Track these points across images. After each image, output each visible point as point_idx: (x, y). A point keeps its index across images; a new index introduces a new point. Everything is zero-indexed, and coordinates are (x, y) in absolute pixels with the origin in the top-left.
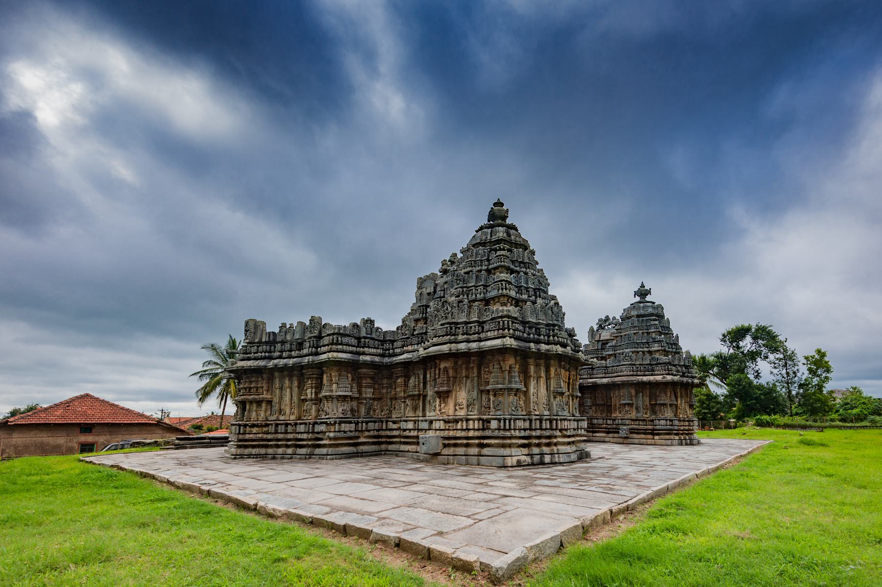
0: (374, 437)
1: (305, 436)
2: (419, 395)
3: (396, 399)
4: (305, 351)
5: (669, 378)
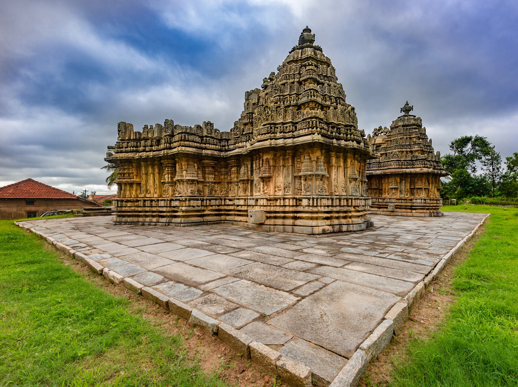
0: (216, 210)
1: (164, 209)
2: (248, 180)
3: (231, 183)
4: (162, 146)
5: (425, 170)
